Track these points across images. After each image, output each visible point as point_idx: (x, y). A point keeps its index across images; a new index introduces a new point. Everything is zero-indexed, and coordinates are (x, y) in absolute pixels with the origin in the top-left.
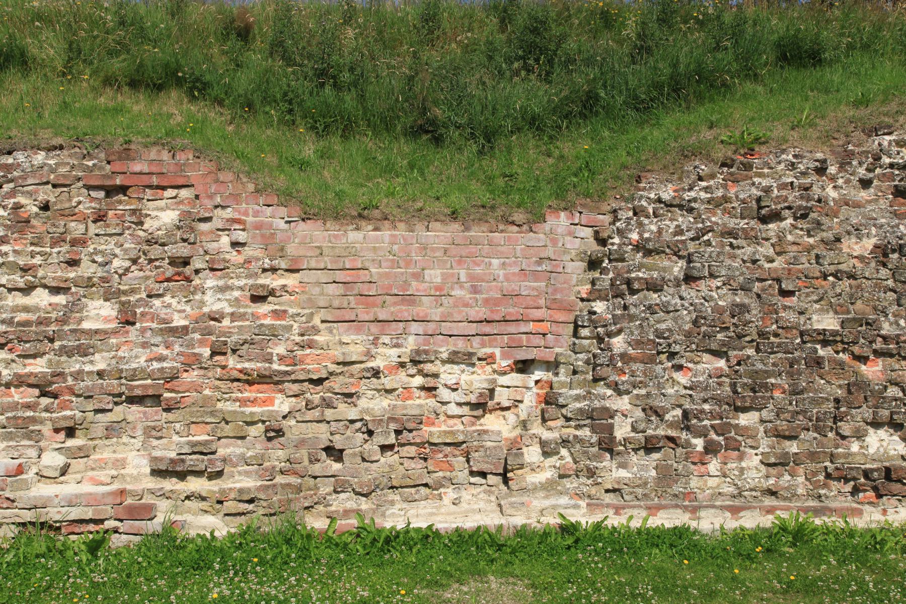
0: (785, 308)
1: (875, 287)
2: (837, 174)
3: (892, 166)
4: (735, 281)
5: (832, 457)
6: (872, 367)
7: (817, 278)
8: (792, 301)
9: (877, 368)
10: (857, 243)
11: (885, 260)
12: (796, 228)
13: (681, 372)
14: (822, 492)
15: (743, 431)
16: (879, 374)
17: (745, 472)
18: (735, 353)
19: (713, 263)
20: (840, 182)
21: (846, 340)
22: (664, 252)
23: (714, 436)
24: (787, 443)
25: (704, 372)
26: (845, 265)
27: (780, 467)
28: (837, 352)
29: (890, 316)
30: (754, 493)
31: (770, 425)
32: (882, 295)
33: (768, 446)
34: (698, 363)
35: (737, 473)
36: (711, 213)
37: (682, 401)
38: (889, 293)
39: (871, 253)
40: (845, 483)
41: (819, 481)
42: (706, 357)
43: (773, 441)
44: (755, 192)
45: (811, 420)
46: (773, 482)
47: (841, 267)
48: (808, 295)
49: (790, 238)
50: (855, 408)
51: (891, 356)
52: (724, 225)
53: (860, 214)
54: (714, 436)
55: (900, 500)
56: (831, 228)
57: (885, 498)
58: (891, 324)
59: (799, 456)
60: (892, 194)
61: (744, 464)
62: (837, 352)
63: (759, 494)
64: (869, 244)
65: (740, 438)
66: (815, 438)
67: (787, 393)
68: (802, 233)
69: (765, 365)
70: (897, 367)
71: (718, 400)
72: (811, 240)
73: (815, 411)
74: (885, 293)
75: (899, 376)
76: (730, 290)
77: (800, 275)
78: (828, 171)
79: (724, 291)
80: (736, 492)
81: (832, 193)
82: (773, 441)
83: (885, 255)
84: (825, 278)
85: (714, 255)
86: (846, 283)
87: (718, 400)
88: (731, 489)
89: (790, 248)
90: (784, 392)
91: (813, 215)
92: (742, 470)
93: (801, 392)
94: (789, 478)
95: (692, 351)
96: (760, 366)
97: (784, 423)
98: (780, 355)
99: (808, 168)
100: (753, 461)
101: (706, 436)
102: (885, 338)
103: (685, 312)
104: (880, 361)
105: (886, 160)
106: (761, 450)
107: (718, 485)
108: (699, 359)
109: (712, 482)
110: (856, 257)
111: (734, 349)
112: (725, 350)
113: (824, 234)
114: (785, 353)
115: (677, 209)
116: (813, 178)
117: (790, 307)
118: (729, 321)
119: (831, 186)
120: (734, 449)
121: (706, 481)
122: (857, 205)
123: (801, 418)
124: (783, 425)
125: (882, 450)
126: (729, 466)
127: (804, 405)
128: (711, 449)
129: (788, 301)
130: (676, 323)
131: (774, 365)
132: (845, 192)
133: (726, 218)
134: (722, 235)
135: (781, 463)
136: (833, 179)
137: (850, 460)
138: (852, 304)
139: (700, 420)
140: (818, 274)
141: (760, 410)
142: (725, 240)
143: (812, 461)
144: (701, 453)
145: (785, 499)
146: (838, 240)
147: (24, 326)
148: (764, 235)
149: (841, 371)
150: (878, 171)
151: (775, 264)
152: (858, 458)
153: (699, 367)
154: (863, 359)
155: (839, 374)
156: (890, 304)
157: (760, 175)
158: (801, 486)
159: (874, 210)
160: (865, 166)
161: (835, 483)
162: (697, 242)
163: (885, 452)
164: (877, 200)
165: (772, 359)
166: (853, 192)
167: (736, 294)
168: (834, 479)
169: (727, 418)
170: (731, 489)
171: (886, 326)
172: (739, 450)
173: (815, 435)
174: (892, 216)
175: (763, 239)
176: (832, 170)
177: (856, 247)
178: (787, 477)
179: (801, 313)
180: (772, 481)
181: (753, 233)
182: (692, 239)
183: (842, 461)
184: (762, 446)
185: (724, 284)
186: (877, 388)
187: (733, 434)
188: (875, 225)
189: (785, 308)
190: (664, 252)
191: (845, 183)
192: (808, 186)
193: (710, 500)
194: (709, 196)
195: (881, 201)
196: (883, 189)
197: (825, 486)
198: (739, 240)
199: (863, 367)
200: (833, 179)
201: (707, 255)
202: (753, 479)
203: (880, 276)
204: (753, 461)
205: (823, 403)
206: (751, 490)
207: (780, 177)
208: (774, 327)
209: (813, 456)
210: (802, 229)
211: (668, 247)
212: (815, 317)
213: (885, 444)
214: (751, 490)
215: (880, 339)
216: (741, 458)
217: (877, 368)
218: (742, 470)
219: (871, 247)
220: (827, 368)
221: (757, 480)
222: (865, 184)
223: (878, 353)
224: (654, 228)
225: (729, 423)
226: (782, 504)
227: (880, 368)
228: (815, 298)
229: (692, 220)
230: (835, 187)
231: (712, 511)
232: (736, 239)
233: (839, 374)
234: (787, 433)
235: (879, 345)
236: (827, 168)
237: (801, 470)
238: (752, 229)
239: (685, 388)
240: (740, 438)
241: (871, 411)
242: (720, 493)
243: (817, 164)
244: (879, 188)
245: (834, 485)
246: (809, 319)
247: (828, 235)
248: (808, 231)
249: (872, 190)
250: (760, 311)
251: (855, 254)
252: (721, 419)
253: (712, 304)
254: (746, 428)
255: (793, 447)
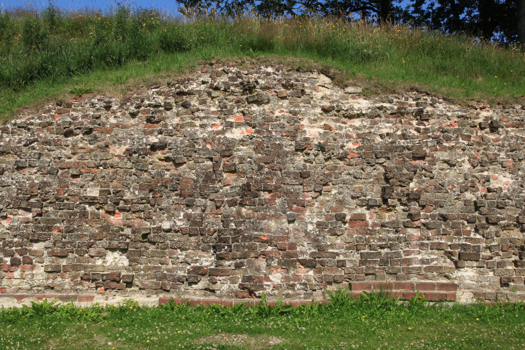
0: (72, 184)
1: (124, 173)
2: (117, 109)
3: (150, 105)
4: (45, 169)
5: (85, 268)
6: (117, 217)
7: (93, 168)
8: (78, 181)
9: (120, 218)
10: (118, 148)
11: (130, 157)
12: (84, 140)
13: (6, 220)
14: (78, 287)
15: (34, 253)
16: (120, 221)
17: (35, 276)
18: (35, 209)
19: (32, 159)
20: (119, 114)
21: (100, 202)
22: (10, 153)
23: (17, 256)
24: (61, 260)
25: (19, 220)
26: (111, 160)
27: (55, 274)
28: (98, 209)
29: (131, 189)
30: (40, 288)
31: (50, 250)
32: (128, 177)
33: (50, 262)
34: (15, 215)
35: (30, 277)
36: (40, 131)
37: (5, 236)
38: (133, 176)
39: (124, 153)
40: (92, 282)
41: (77, 281)
42: (21, 212)
43: (53, 259)
44: (69, 119)
45: (75, 247)
46: (51, 282)
47: (108, 162)
48: (86, 177)
49: (81, 145)
50: (98, 240)
51: (128, 211)
52: (46, 138)
53: (125, 132)
54: (17, 256)
55: (117, 292)
56: (103, 140)
57: (108, 290)
58: (131, 193)
59: (65, 267)
60: (146, 121)
61: (34, 272)
62: (98, 209)
63: (43, 288)
64: (124, 148)
65: (32, 257)
66: (76, 257)
67: (64, 232)
68: (86, 142)
69: (56, 216)
70: (130, 217)
71: (22, 236)
72: (92, 147)
73: (77, 242)
74: (130, 176)
75: (131, 222)
76: (41, 174)
77: (84, 166)
78: (112, 108)
79: (38, 174)
80: (30, 287)
81: (113, 120)
82: (53, 259)
83: (131, 155)
84: (98, 168)
85: (32, 154)
86: (111, 170)
87: (22, 236)
88: (27, 286)
89: (79, 151)
90: (60, 231)
91: (94, 133)
92: (33, 275)
93: (72, 231)
94: (61, 279)
95: (11, 208)
96: (53, 217)
97: (59, 248)
98: (65, 211)
99: (101, 106)
100: (40, 271)
101: (12, 256)
102: (126, 202)
103: (14, 187)
104: (121, 214)
105: (147, 102)
106: (45, 264)
107: (19, 284)
108: (16, 213)
109: (15, 282)
110: (116, 156)
111: (35, 207)
112: (29, 207)
113: (99, 143)
114: (68, 209)
115: (23, 129)
116: (103, 112)
117: (74, 184)
118: (37, 191)
119: (113, 116)
120: (28, 263)
121: (12, 282)
122: (125, 127)
123: (69, 246)
124: (58, 250)
125: (114, 264)
126: (26, 273)
127: (72, 238)
128: (15, 263)
129: (75, 181)
130: (8, 192)
131: (60, 216)
132: (121, 120)
133: (48, 134)
134: (43, 143)
135: (55, 271)
136: (114, 112)
137: (94, 269)
138: (111, 182)
139: (10, 247)
140: (94, 165)
141: (44, 241)
142: (44, 146)
143: (73, 270)
144: (9, 266)
145: (58, 291)
146: (107, 146)
147: (93, 200)
148: (65, 144)
149: (97, 219)
150: (142, 108)
151: (72, 160)
152: (99, 268)
153: (16, 217)
154: (112, 213)
155: (96, 221)
156: (133, 182)
157: (74, 110)
158: (67, 284)
159: (133, 130)
160: (134, 105)
161: (87, 282)
162: (28, 147)
163: (116, 265)
164: (138, 124)
165: (60, 213)
166: (126, 120)
167: (45, 177)
168: (85, 280)
169: (26, 246)
170: (27, 286)
171: (128, 194)
172: (32, 264)
173: (77, 255)
174: (143, 133)
175: (65, 146)
176: (114, 107)
177: (118, 150)
178: (59, 279)
179: (82, 187)
180: (50, 281)
181: (59, 143)
182: (25, 146)
183: (89, 270)
184: (45, 262)
185: (38, 171)
186: (115, 229)
187: (28, 255)
188: (130, 138)
189: (72, 184)
190: (10, 153)
191: (122, 115)
192: (98, 116)
193: (14, 292)
194: (40, 121)
195: (140, 125)
196: (142, 118)
197: (81, 284)
198: (52, 146)
199: (112, 217)
200: (114, 112)
201: (28, 155)
202: (39, 280)
203: (127, 166)
204: (40, 271)
205: (83, 237)
206: (38, 286)
207: (87, 111)
208: (66, 195)
209: (75, 267)
210: (86, 140)
211: (12, 150)
212: (88, 189)
213: (117, 260)
214: (38, 286)
215: (123, 202)
216: (33, 268)
217: (120, 218)
218: (33, 275)
219: (124, 150)
220: (89, 218)
221: (41, 281)
222: (133, 115)
223: (122, 210)
224: (8, 139)
225: (26, 249)
226: (56, 294)
227: (121, 218)
228: (90, 178)
229: (30, 135)
230: (115, 117)
231: (6, 298)
232: (50, 146)
233: (96, 221)
234: (59, 254)
235: (121, 204)
236: (111, 107)
237: (67, 275)
238: (59, 140)
239: (7, 229)
240: (32, 257)
241: (108, 242)
242: (20, 288)
243: (105, 104)
244: (140, 118)
245: (86, 283)
246: (85, 190)
247: (102, 143)
248: (89, 141)
249: (137, 119)
250: (58, 186)
251: (116, 154)
252: (22, 247)
253: (30, 182)
254: (36, 251)
255: (64, 262)
